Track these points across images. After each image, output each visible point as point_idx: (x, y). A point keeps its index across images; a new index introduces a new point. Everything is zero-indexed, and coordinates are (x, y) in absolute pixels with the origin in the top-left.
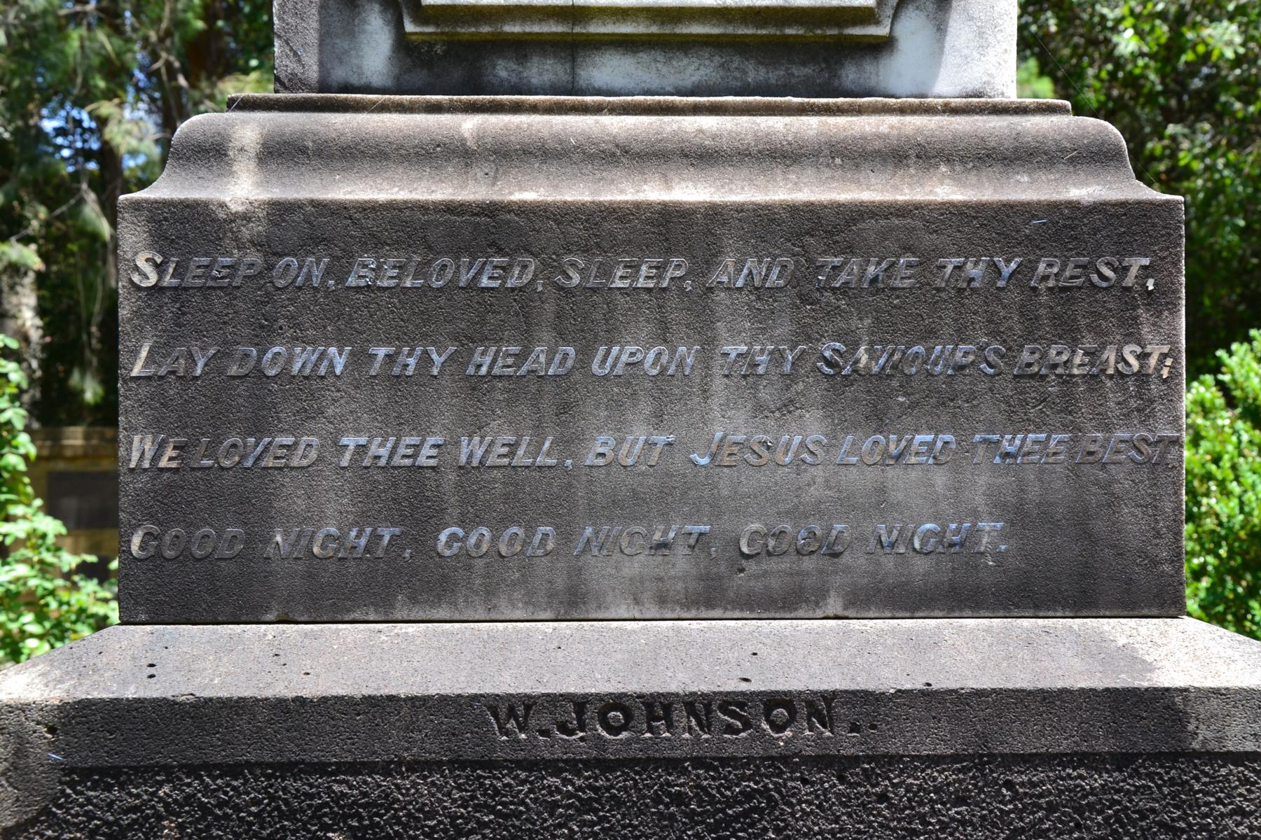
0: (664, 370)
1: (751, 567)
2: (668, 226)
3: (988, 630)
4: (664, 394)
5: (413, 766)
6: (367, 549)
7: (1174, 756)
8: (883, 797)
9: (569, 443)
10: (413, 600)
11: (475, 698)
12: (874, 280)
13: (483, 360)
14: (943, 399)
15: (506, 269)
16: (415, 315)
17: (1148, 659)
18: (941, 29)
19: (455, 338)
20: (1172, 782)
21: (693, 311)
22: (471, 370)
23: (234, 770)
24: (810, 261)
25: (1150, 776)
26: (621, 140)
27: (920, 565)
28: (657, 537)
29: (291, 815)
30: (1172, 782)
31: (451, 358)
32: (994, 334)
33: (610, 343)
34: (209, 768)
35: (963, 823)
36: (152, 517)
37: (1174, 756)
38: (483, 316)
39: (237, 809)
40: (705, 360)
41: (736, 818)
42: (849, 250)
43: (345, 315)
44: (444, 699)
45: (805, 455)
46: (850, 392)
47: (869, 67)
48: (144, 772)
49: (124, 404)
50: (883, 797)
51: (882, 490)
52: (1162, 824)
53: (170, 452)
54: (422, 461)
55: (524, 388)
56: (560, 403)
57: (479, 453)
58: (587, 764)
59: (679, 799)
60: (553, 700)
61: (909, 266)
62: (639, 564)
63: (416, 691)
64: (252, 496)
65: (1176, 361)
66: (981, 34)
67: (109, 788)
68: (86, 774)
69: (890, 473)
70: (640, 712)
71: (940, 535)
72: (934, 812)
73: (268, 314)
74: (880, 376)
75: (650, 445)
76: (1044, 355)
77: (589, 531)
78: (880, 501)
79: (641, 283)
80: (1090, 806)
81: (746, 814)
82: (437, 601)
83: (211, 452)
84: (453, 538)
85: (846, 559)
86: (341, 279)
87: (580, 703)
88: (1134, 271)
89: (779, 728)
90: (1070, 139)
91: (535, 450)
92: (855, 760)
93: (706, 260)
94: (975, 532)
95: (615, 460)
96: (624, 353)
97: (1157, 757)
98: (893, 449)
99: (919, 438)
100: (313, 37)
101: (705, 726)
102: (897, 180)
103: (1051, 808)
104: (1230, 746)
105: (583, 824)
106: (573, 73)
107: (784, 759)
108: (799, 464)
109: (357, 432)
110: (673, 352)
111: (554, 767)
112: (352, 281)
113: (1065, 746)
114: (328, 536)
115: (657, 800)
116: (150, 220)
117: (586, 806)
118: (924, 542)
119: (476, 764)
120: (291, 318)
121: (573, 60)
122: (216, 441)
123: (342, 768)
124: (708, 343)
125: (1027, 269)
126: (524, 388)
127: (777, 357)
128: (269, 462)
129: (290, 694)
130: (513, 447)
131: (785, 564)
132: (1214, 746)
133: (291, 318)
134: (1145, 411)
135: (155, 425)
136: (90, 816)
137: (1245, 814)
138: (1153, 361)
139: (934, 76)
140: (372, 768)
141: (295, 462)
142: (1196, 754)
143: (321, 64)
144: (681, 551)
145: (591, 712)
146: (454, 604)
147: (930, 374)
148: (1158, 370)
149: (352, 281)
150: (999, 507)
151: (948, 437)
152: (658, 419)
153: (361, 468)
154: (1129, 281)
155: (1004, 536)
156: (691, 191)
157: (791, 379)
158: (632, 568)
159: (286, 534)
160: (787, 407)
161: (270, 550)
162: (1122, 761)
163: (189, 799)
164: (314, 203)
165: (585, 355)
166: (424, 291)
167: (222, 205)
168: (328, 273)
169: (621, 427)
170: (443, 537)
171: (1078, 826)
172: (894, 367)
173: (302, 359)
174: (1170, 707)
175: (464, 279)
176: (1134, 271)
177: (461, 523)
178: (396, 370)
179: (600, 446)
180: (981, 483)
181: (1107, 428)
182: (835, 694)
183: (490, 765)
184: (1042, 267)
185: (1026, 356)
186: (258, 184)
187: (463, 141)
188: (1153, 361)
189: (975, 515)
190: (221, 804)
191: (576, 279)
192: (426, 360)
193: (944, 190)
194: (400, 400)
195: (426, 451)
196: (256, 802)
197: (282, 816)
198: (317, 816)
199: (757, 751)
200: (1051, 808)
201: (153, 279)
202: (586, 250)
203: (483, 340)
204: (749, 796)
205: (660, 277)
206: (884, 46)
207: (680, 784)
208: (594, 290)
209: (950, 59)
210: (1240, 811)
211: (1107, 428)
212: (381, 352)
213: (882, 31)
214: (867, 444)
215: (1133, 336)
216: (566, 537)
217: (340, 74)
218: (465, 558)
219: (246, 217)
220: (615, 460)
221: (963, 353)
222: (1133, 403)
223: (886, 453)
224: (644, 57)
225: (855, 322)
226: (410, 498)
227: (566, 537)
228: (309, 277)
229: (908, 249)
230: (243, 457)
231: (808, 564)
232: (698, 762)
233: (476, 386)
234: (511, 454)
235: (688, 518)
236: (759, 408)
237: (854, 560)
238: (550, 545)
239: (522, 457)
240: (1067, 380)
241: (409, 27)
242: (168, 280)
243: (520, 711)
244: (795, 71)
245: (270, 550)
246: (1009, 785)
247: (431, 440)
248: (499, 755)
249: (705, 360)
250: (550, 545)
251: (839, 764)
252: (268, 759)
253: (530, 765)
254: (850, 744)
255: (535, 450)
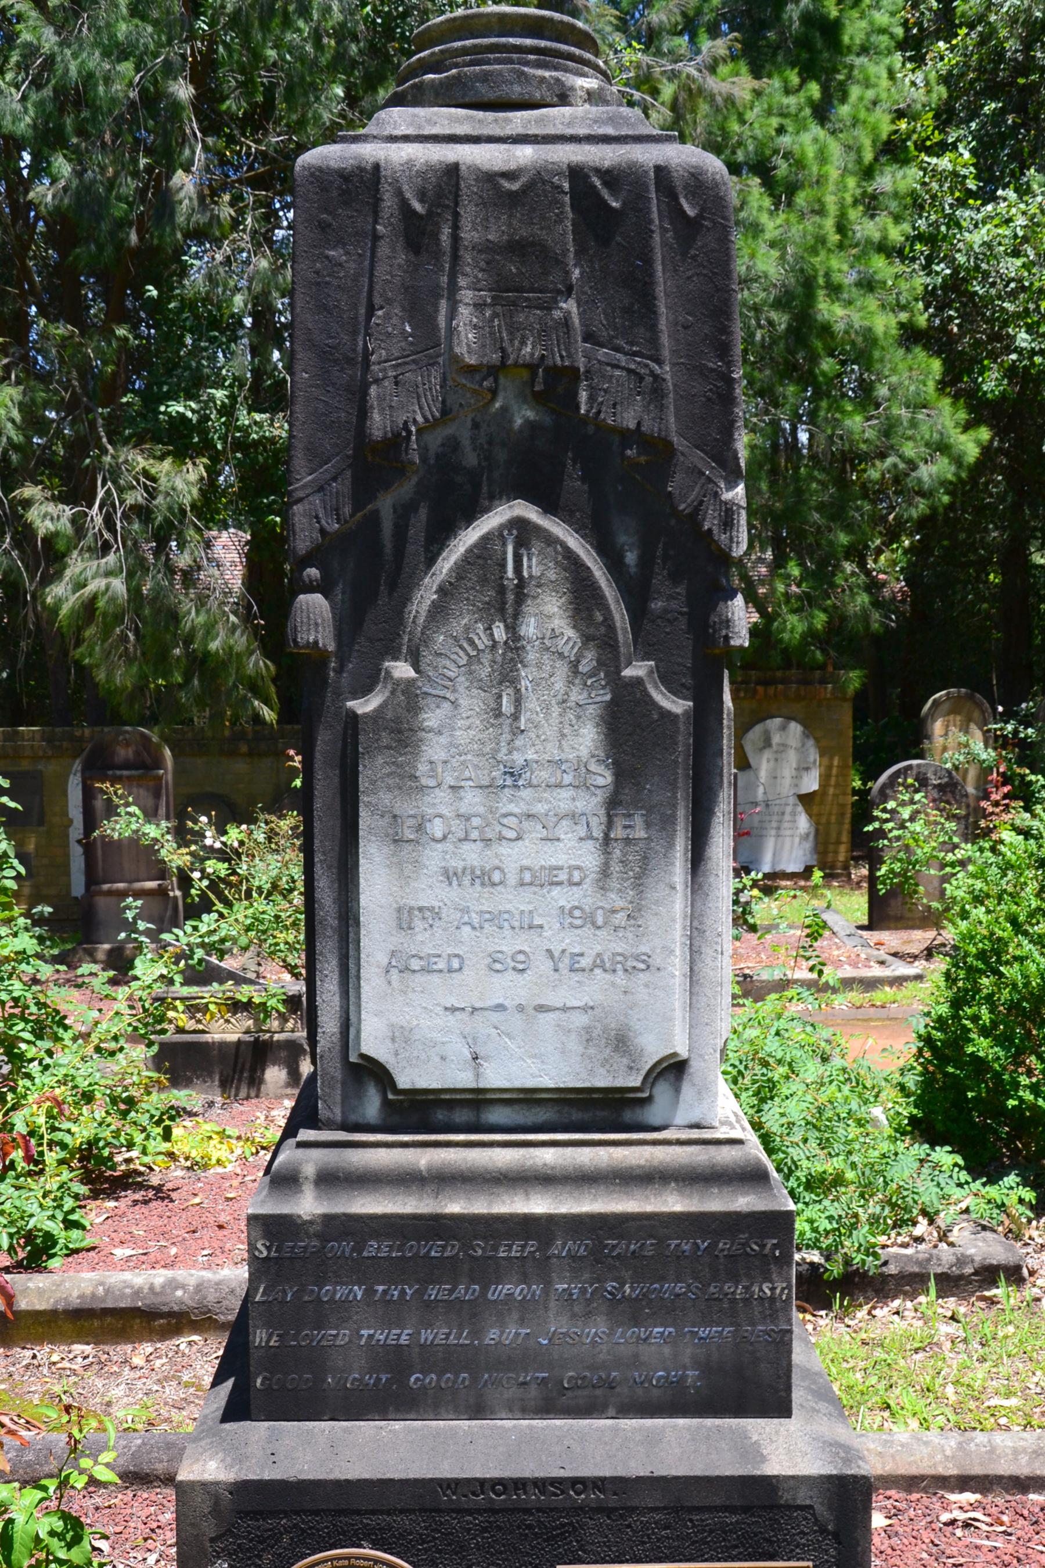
0: (525, 1297)
1: (570, 1394)
2: (527, 1224)
3: (689, 1428)
4: (526, 1309)
5: (402, 1511)
6: (374, 1385)
7: (771, 1507)
8: (629, 1526)
9: (476, 1333)
10: (397, 1410)
11: (431, 1480)
12: (634, 1252)
13: (433, 1293)
14: (668, 1310)
15: (444, 1247)
16: (398, 1270)
17: (765, 1452)
18: (677, 1090)
19: (418, 1281)
20: (770, 1519)
21: (538, 1268)
22: (426, 1297)
23: (316, 1513)
24: (601, 1242)
25: (760, 1516)
26: (503, 1171)
27: (656, 1392)
28: (521, 1379)
29: (344, 1533)
30: (770, 1519)
31: (416, 1291)
32: (696, 1279)
33: (498, 1284)
34: (305, 1512)
35: (668, 1538)
36: (266, 1370)
37: (771, 1507)
38: (431, 1271)
39: (318, 1530)
40: (546, 1292)
41: (557, 1535)
42: (621, 1237)
43: (364, 1271)
44: (416, 1480)
45: (595, 1337)
46: (621, 1307)
47: (638, 1111)
48: (274, 1514)
49: (252, 1314)
50: (629, 1526)
51: (636, 1356)
52: (765, 1539)
53: (275, 1338)
54: (402, 1342)
55: (453, 1307)
56: (472, 1313)
57: (431, 1338)
58: (485, 1511)
59: (530, 1527)
60: (469, 1481)
61: (652, 1245)
62: (511, 1392)
63: (403, 1476)
64: (315, 1360)
65: (790, 1291)
66: (699, 1093)
67: (258, 1520)
68: (247, 1513)
69: (641, 1347)
70: (511, 1487)
71: (667, 1377)
72: (654, 1533)
73: (321, 1267)
74: (636, 1299)
75: (517, 1334)
76: (722, 1289)
77: (486, 1376)
78: (635, 1361)
79: (513, 1254)
80: (730, 1531)
81: (562, 1534)
82: (409, 1411)
83: (295, 1337)
84: (417, 1379)
85: (618, 1390)
86: (360, 1253)
87: (482, 1482)
88: (769, 1246)
89: (578, 1494)
90: (740, 1167)
91: (459, 1336)
92: (616, 1509)
93: (546, 1243)
94: (684, 1377)
95: (499, 1342)
96: (506, 1288)
97: (764, 1508)
98: (643, 1336)
99: (656, 1330)
100: (338, 1098)
101: (542, 1493)
102: (648, 1192)
103: (711, 1531)
104: (799, 1502)
105: (483, 1538)
106: (478, 1116)
107: (581, 1508)
108: (594, 1343)
109: (369, 1328)
110: (529, 1288)
111: (469, 1512)
112: (365, 1254)
113: (718, 1502)
114: (355, 1379)
115: (519, 1527)
116: (264, 1224)
117: (485, 1530)
118: (658, 1381)
119: (431, 1511)
120: (335, 1272)
121: (478, 1110)
122: (298, 1332)
123: (367, 1512)
124: (548, 1283)
125: (713, 1246)
126: (453, 1307)
127: (583, 1291)
128: (324, 1343)
129: (343, 1478)
130: (448, 1335)
131: (586, 1392)
132: (791, 1502)
133: (335, 1272)
134: (773, 1317)
135: (268, 1325)
136: (250, 1533)
137: (805, 1534)
138: (778, 1291)
139: (674, 1116)
140: (382, 1512)
141: (338, 1343)
142: (782, 1506)
143: (343, 1112)
144: (534, 1386)
145: (487, 1486)
146: (418, 1412)
147: (662, 1298)
148: (781, 1295)
149: (365, 1254)
150: (696, 1364)
151: (671, 1329)
152: (522, 1322)
153: (371, 1346)
154: (767, 1250)
155: (699, 1378)
156: (538, 1204)
157: (589, 1302)
158: (508, 1394)
159: (333, 1378)
160: (588, 1314)
161: (325, 1386)
162: (746, 1510)
163: (295, 1526)
164: (345, 1215)
165: (485, 1289)
166: (403, 1257)
167: (299, 1216)
168: (353, 1250)
169: (503, 1326)
170: (412, 1379)
171: (724, 1540)
172: (644, 1295)
173: (341, 1292)
174: (770, 1484)
175: (423, 1252)
176: (769, 1246)
177: (421, 1372)
178: (388, 1298)
179: (493, 1334)
180: (687, 1353)
181: (753, 1324)
182: (605, 1478)
183: (439, 1511)
184: (721, 1245)
185: (712, 1289)
186: (318, 1198)
187: (421, 1171)
188: (778, 1291)
189: (685, 1368)
190: (310, 1528)
191: (480, 1252)
192: (403, 1292)
193: (673, 1202)
194: (391, 1313)
195: (404, 1337)
196: (327, 1527)
197: (339, 1534)
198: (356, 1534)
199: (568, 1504)
200: (711, 1531)
201: (265, 1253)
202: (484, 1238)
203: (433, 1282)
204: (563, 1525)
205: (522, 1251)
206: (649, 1099)
207: (530, 1520)
208: (489, 1258)
209: (682, 1105)
210: (802, 1532)
211: (753, 1324)
212: (381, 1288)
213: (646, 1095)
214: (629, 1333)
215: (768, 1279)
216: (475, 1379)
217: (353, 1118)
218: (424, 1389)
219: (311, 1222)
220: (499, 1342)
221: (680, 1288)
222: (768, 1312)
223: (639, 1337)
224: (516, 1107)
225: (623, 1273)
226: (396, 1361)
227: (475, 1379)
228: (343, 1252)
229: (651, 1236)
230: (312, 1341)
231: (598, 1392)
232: (539, 1510)
233: (429, 1306)
234: (447, 1338)
235: (537, 1370)
236: (574, 1316)
237: (623, 1390)
238: (467, 1383)
239: (452, 1340)
240: (733, 1301)
241: (390, 1096)
242: (273, 1254)
243: (453, 1486)
244: (598, 1113)
245: (325, 1386)
246: (691, 1520)
247: (406, 1332)
248: (443, 1506)
249: (546, 1292)
250: (467, 1383)
251: (608, 1511)
252: (332, 1507)
253: (458, 1511)
254: (613, 1501)
255: (459, 1336)
